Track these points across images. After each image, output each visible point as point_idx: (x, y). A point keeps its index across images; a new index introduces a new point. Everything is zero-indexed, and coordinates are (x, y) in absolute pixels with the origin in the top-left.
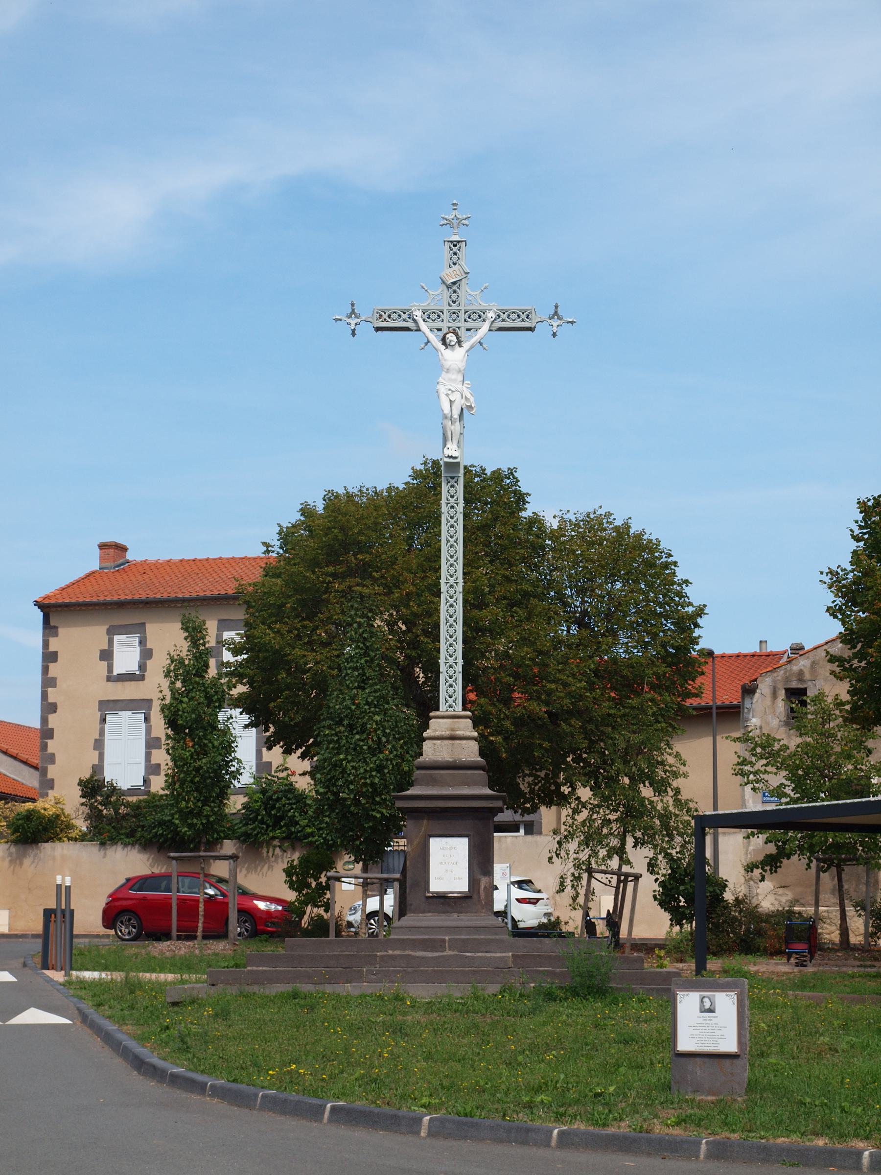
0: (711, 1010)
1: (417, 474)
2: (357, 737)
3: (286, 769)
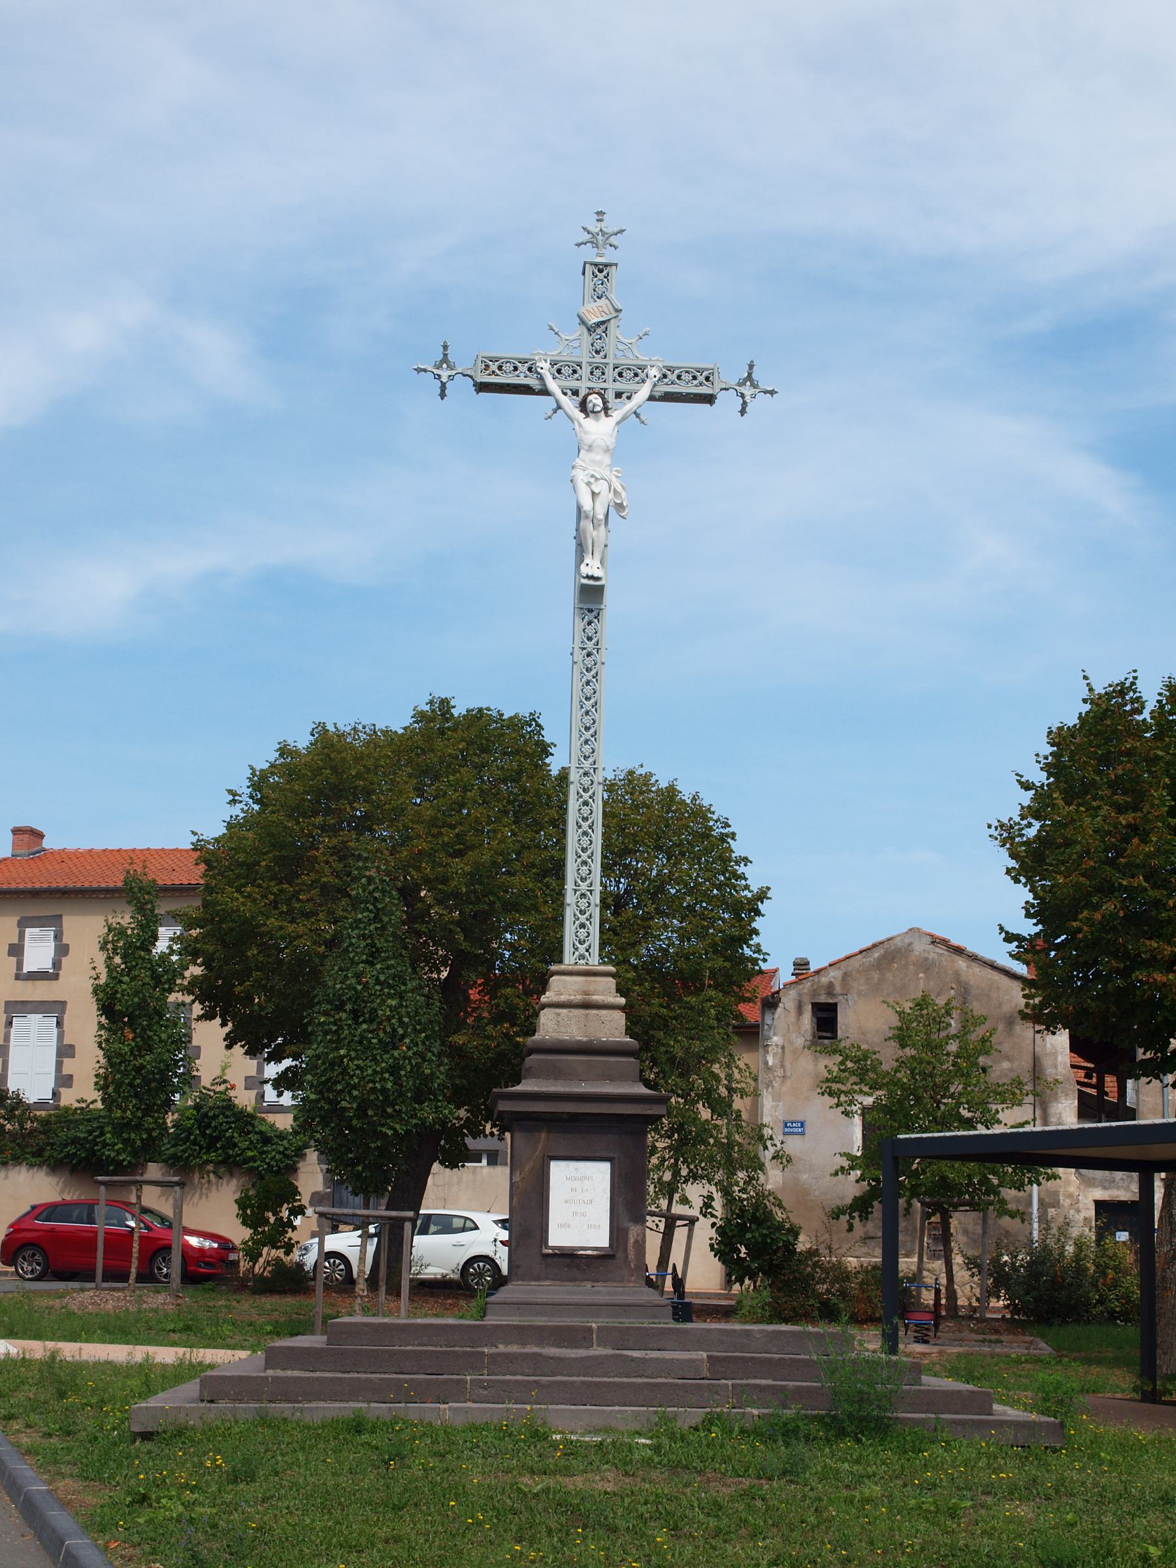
1: (420, 716)
2: (364, 1026)
3: (225, 1082)
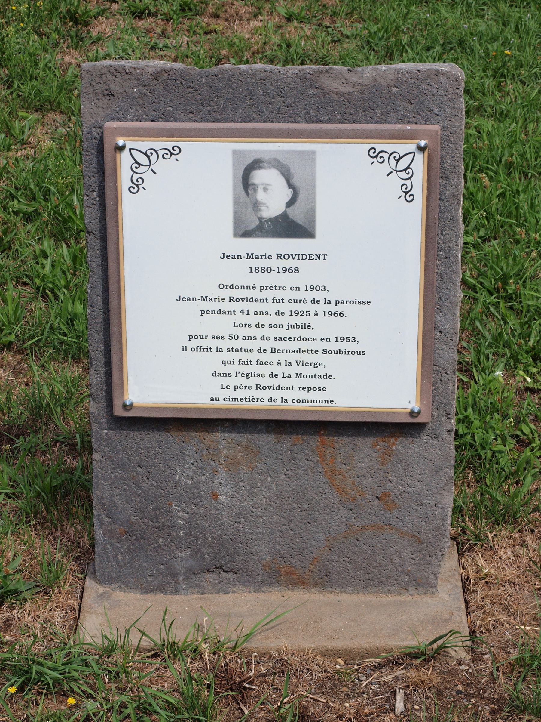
0: (290, 226)
